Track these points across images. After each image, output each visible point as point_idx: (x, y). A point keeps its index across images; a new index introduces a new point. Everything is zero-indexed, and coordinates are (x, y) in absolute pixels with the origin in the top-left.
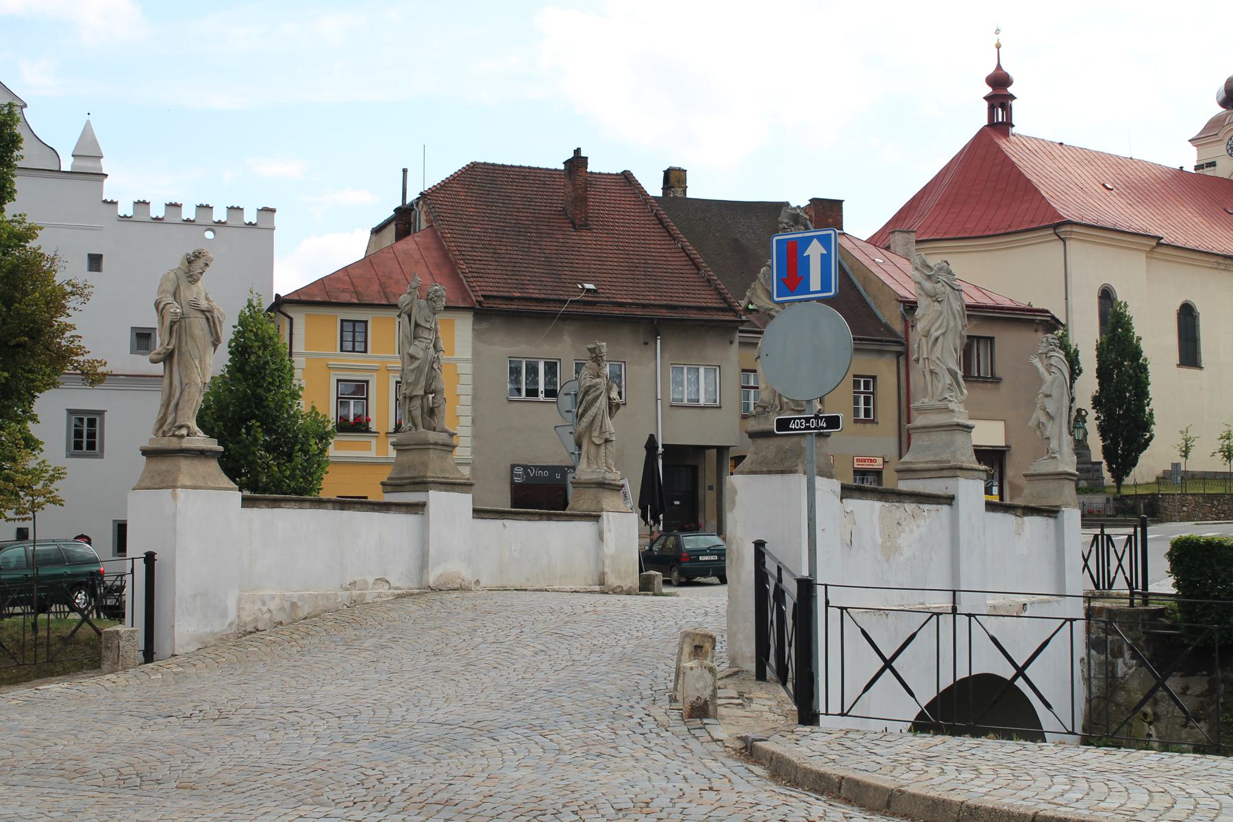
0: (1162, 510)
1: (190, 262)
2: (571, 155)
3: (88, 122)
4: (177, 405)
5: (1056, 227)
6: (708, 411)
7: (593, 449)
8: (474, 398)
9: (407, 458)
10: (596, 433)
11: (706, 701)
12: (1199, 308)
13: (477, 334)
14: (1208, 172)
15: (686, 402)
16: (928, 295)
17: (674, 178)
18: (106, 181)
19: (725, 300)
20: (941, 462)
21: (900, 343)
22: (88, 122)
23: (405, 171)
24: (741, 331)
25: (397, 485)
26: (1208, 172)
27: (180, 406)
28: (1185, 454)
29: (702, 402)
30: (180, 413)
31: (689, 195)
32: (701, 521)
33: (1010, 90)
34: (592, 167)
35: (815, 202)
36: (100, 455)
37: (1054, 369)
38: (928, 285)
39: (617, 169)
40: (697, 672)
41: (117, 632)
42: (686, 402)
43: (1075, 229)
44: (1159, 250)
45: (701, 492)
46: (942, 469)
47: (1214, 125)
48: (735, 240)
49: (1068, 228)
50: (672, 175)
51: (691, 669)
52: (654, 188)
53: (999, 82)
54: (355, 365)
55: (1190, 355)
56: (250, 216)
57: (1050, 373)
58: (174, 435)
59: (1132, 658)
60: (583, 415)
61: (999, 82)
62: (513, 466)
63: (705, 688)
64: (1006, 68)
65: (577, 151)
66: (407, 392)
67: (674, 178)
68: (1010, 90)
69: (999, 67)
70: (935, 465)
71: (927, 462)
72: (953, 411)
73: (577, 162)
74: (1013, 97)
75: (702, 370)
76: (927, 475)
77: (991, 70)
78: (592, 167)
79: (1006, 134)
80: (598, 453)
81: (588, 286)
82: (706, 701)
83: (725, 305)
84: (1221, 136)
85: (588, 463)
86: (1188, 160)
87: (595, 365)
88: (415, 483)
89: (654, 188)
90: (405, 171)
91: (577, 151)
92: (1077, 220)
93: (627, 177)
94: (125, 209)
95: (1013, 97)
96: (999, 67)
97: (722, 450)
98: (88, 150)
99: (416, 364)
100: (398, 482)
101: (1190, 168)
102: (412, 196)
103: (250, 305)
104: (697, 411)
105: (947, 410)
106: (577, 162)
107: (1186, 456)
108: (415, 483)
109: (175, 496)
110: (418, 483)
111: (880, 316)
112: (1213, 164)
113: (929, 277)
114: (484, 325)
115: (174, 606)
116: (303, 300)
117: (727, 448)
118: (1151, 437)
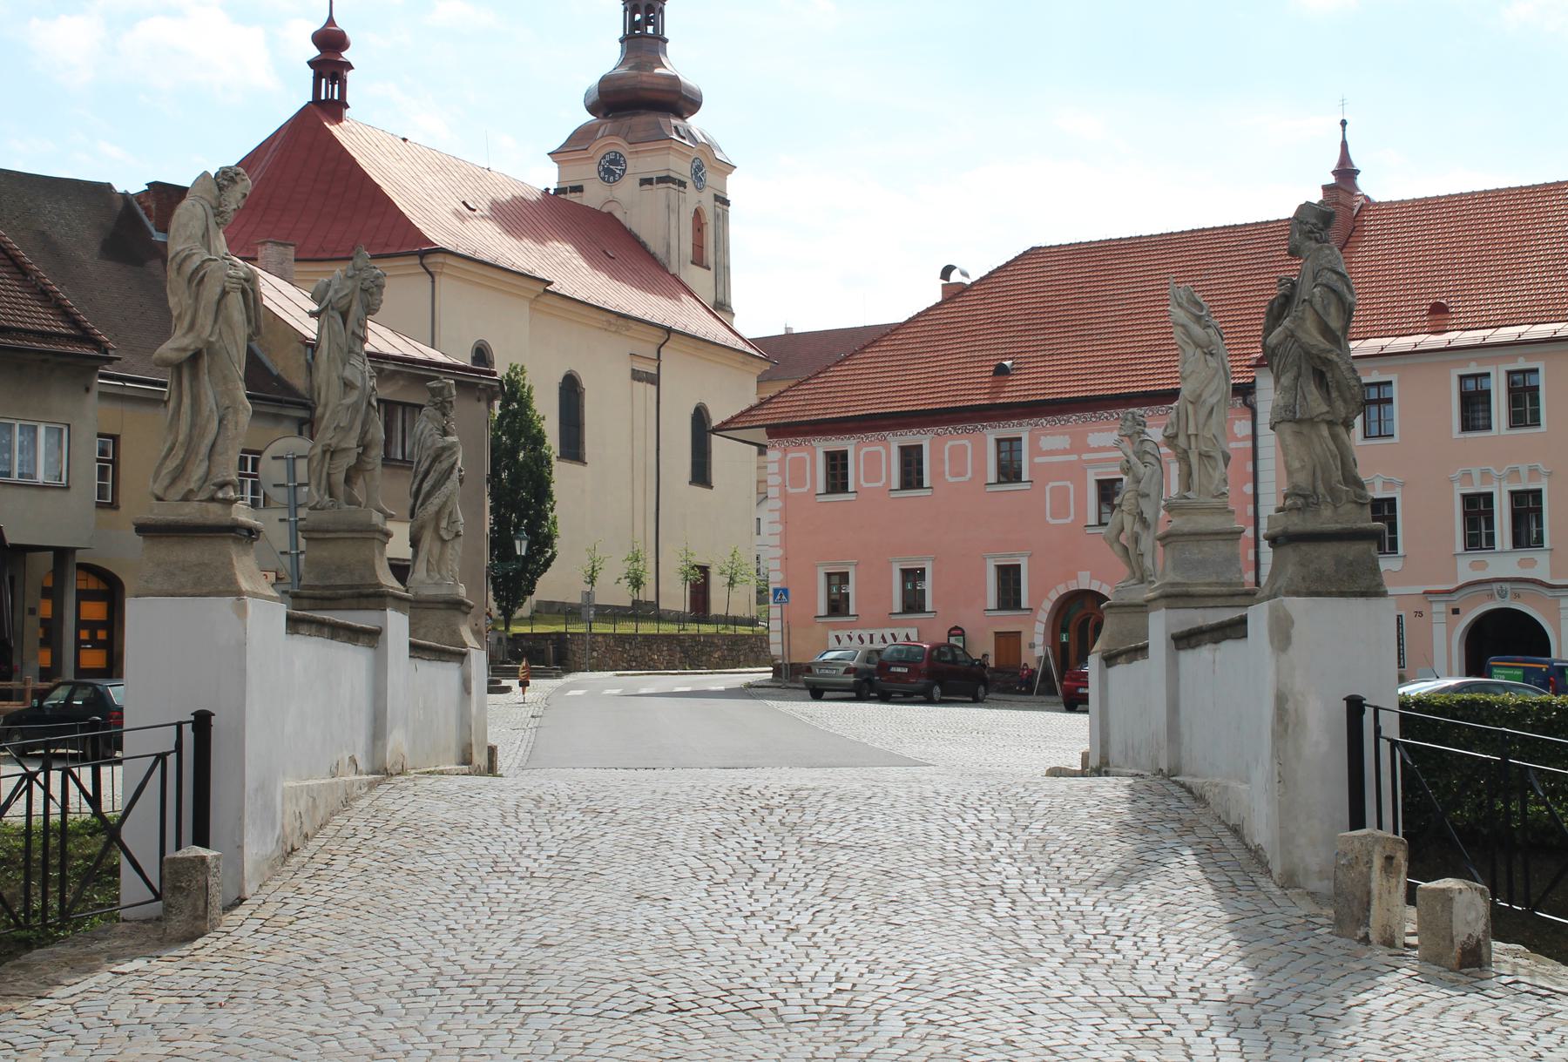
0: (570, 656)
1: (221, 188)
4: (213, 445)
5: (422, 255)
6: (50, 493)
7: (437, 546)
9: (324, 553)
10: (444, 524)
11: (1479, 941)
12: (585, 383)
14: (572, 197)
15: (15, 477)
16: (1198, 345)
19: (76, 323)
20: (1230, 585)
21: (305, 406)
24: (103, 376)
25: (323, 599)
26: (573, 197)
27: (218, 448)
28: (592, 580)
29: (41, 477)
30: (218, 458)
32: (16, 662)
33: (346, 55)
35: (157, 188)
37: (1148, 458)
38: (1197, 330)
40: (1467, 895)
41: (203, 859)
42: (15, 477)
43: (450, 260)
44: (548, 299)
46: (1233, 595)
47: (579, 140)
48: (43, 233)
49: (439, 258)
51: (1460, 891)
53: (330, 43)
55: (573, 449)
57: (1145, 464)
58: (212, 499)
60: (429, 494)
61: (330, 43)
63: (1477, 920)
64: (341, 24)
66: (334, 442)
68: (346, 55)
69: (331, 21)
70: (1225, 590)
71: (1209, 584)
72: (1232, 512)
74: (349, 66)
75: (42, 430)
76: (1219, 601)
77: (319, 24)
79: (338, 118)
80: (442, 553)
82: (1479, 941)
83: (78, 333)
84: (592, 150)
86: (547, 177)
87: (438, 414)
88: (361, 596)
92: (450, 248)
95: (349, 66)
96: (331, 21)
99: (353, 397)
100: (327, 593)
101: (553, 186)
104: (34, 492)
105: (1225, 511)
107: (592, 582)
108: (361, 596)
109: (242, 611)
110: (368, 596)
111: (268, 363)
112: (579, 189)
113: (1198, 319)
115: (242, 809)
117: (72, 550)
118: (553, 556)
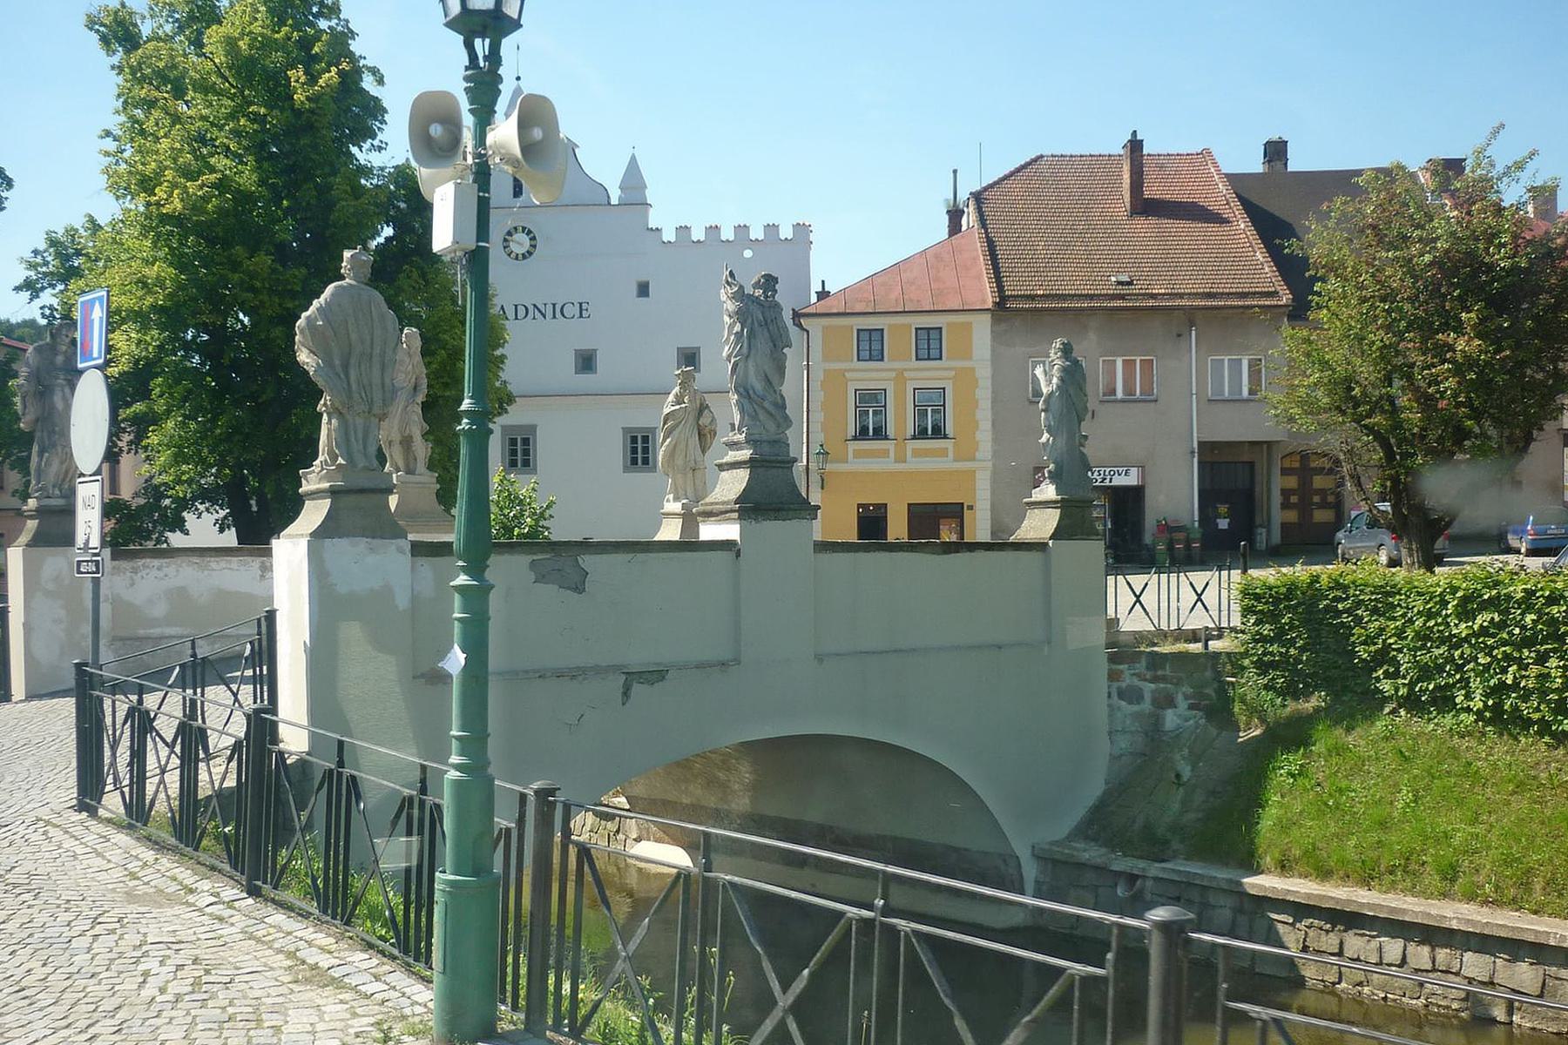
3: (633, 158)
13: (996, 336)
15: (1120, 394)
18: (651, 211)
22: (633, 158)
23: (955, 172)
39: (947, 217)
54: (870, 376)
59: (1191, 707)
90: (955, 172)
94: (669, 235)
98: (633, 178)
114: (1003, 326)
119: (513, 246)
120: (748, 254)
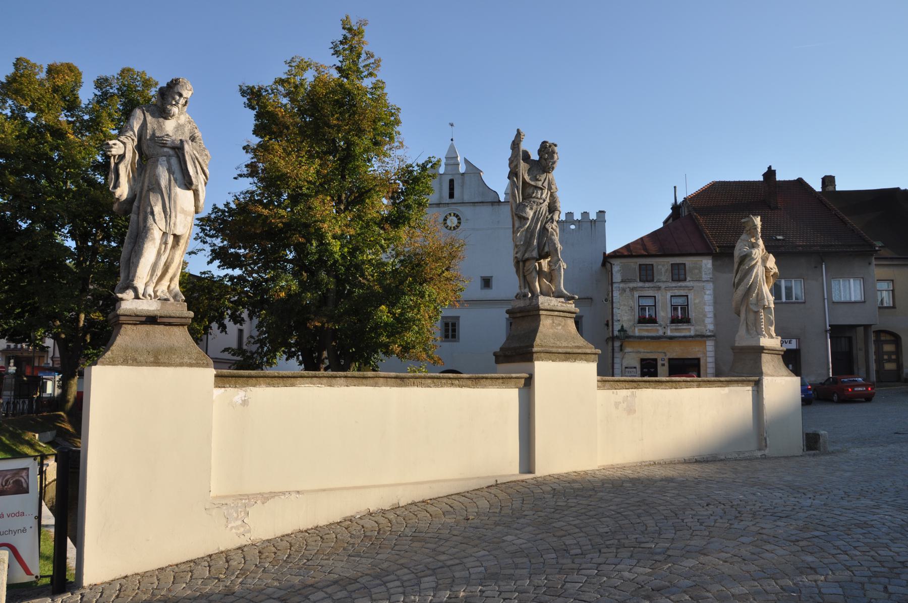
2: (766, 170)
8: (715, 315)
17: (828, 181)
29: (853, 299)
31: (838, 189)
34: (779, 177)
36: (458, 341)
45: (855, 352)
50: (826, 181)
52: (817, 187)
56: (593, 216)
62: (896, 339)
65: (770, 168)
67: (828, 181)
73: (770, 174)
78: (779, 177)
81: (779, 237)
85: (748, 330)
89: (817, 187)
91: (770, 168)
93: (800, 181)
97: (867, 327)
102: (680, 200)
103: (423, 167)
106: (770, 174)
116: (616, 254)
119: (449, 223)
120: (573, 227)
